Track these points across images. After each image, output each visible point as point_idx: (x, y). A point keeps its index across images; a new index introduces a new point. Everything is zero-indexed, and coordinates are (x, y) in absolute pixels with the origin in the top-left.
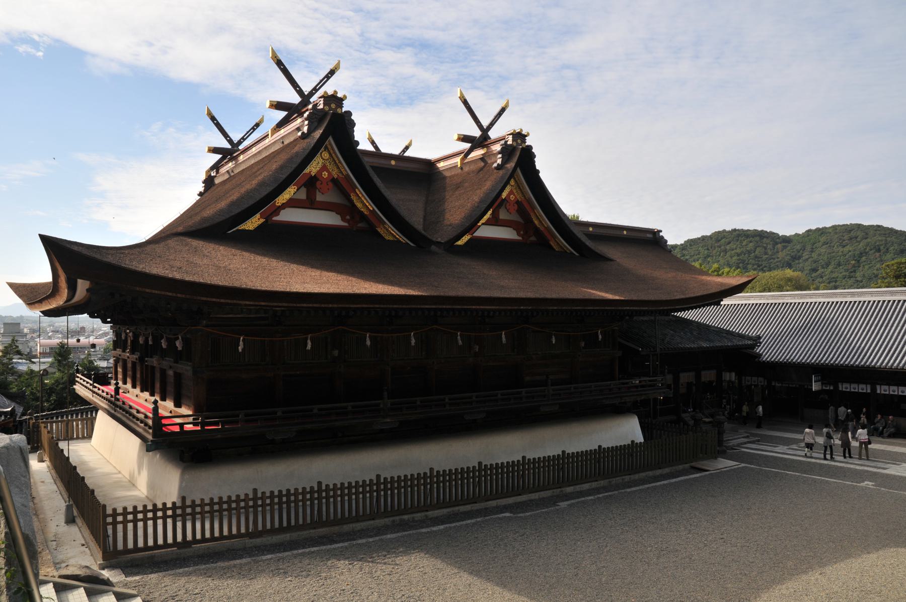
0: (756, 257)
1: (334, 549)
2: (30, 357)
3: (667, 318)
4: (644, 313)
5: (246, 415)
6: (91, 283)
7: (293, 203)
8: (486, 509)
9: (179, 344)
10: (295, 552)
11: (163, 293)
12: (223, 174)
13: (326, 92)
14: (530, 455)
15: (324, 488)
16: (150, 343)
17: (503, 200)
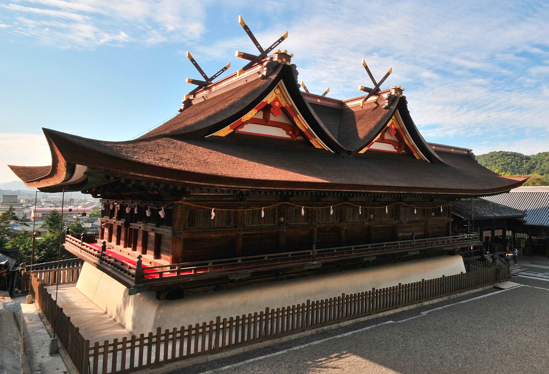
0: (512, 166)
1: (277, 356)
2: (25, 221)
3: (475, 199)
4: (466, 197)
5: (214, 263)
6: (89, 168)
7: (253, 121)
8: (377, 318)
9: (161, 214)
10: (247, 361)
11: (153, 177)
12: (199, 99)
13: (279, 50)
14: (404, 283)
15: (270, 312)
16: (136, 212)
17: (388, 128)
